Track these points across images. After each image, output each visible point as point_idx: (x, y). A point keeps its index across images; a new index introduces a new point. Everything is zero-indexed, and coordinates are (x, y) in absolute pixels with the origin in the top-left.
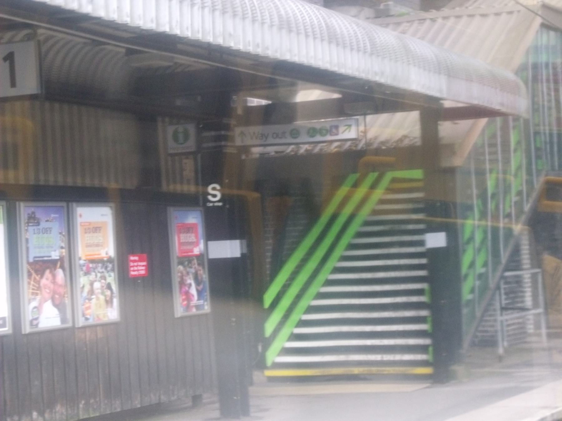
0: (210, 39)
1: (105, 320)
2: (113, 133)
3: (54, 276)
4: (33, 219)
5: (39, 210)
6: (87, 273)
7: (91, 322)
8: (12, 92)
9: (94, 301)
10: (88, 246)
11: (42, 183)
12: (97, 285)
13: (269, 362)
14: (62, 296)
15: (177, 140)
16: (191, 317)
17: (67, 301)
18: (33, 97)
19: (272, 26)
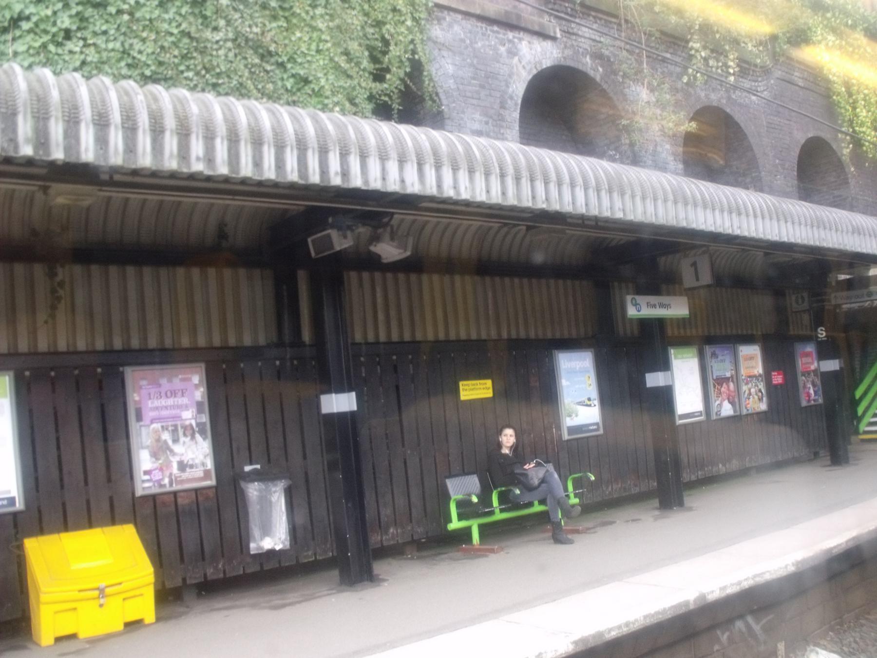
0: (812, 243)
1: (758, 410)
2: (764, 302)
3: (728, 387)
4: (714, 355)
5: (717, 349)
6: (747, 384)
7: (750, 412)
8: (696, 284)
9: (751, 399)
10: (747, 368)
11: (712, 334)
12: (753, 390)
13: (861, 430)
14: (734, 398)
15: (798, 303)
16: (811, 406)
17: (736, 400)
18: (709, 286)
19: (847, 232)
